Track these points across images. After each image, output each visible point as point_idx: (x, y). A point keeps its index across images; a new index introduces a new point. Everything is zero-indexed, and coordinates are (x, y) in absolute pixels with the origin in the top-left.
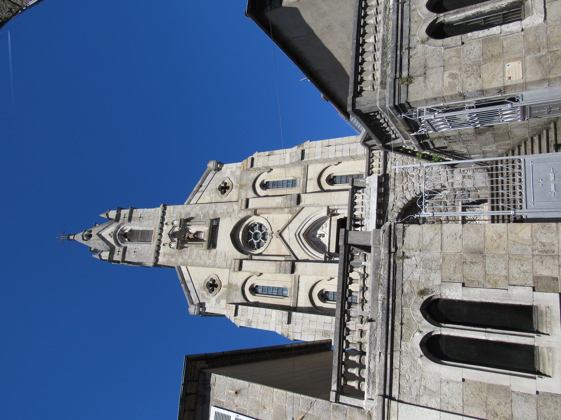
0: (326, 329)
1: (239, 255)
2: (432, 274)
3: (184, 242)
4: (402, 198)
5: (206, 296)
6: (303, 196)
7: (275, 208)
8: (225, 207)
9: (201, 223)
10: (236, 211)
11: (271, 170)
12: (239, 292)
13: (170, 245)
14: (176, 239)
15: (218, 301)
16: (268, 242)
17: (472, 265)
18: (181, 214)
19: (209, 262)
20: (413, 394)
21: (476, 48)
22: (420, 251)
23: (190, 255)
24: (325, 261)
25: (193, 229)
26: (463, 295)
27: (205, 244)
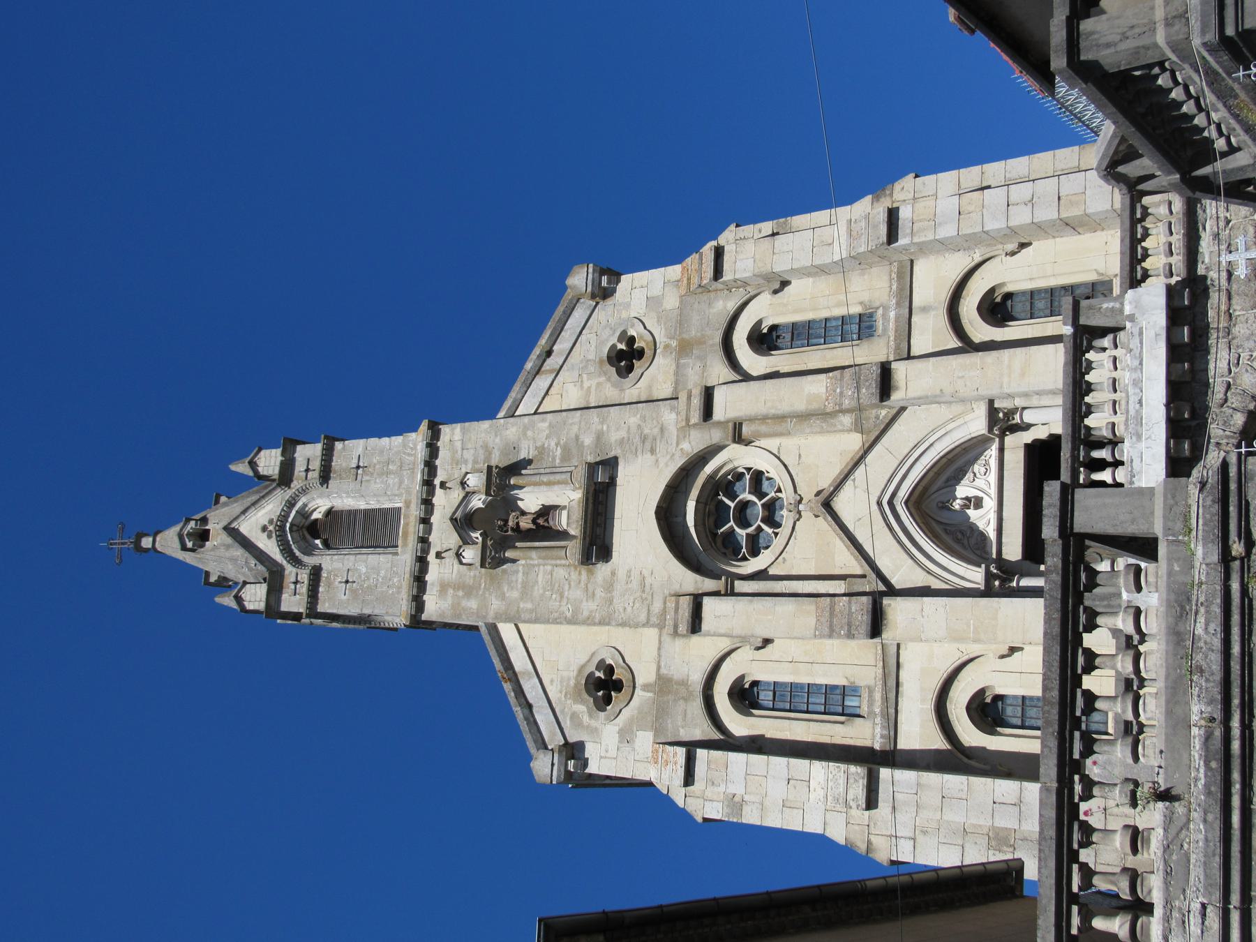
9: (558, 477)
13: (458, 555)
14: (476, 535)
25: (531, 500)
27: (574, 548)
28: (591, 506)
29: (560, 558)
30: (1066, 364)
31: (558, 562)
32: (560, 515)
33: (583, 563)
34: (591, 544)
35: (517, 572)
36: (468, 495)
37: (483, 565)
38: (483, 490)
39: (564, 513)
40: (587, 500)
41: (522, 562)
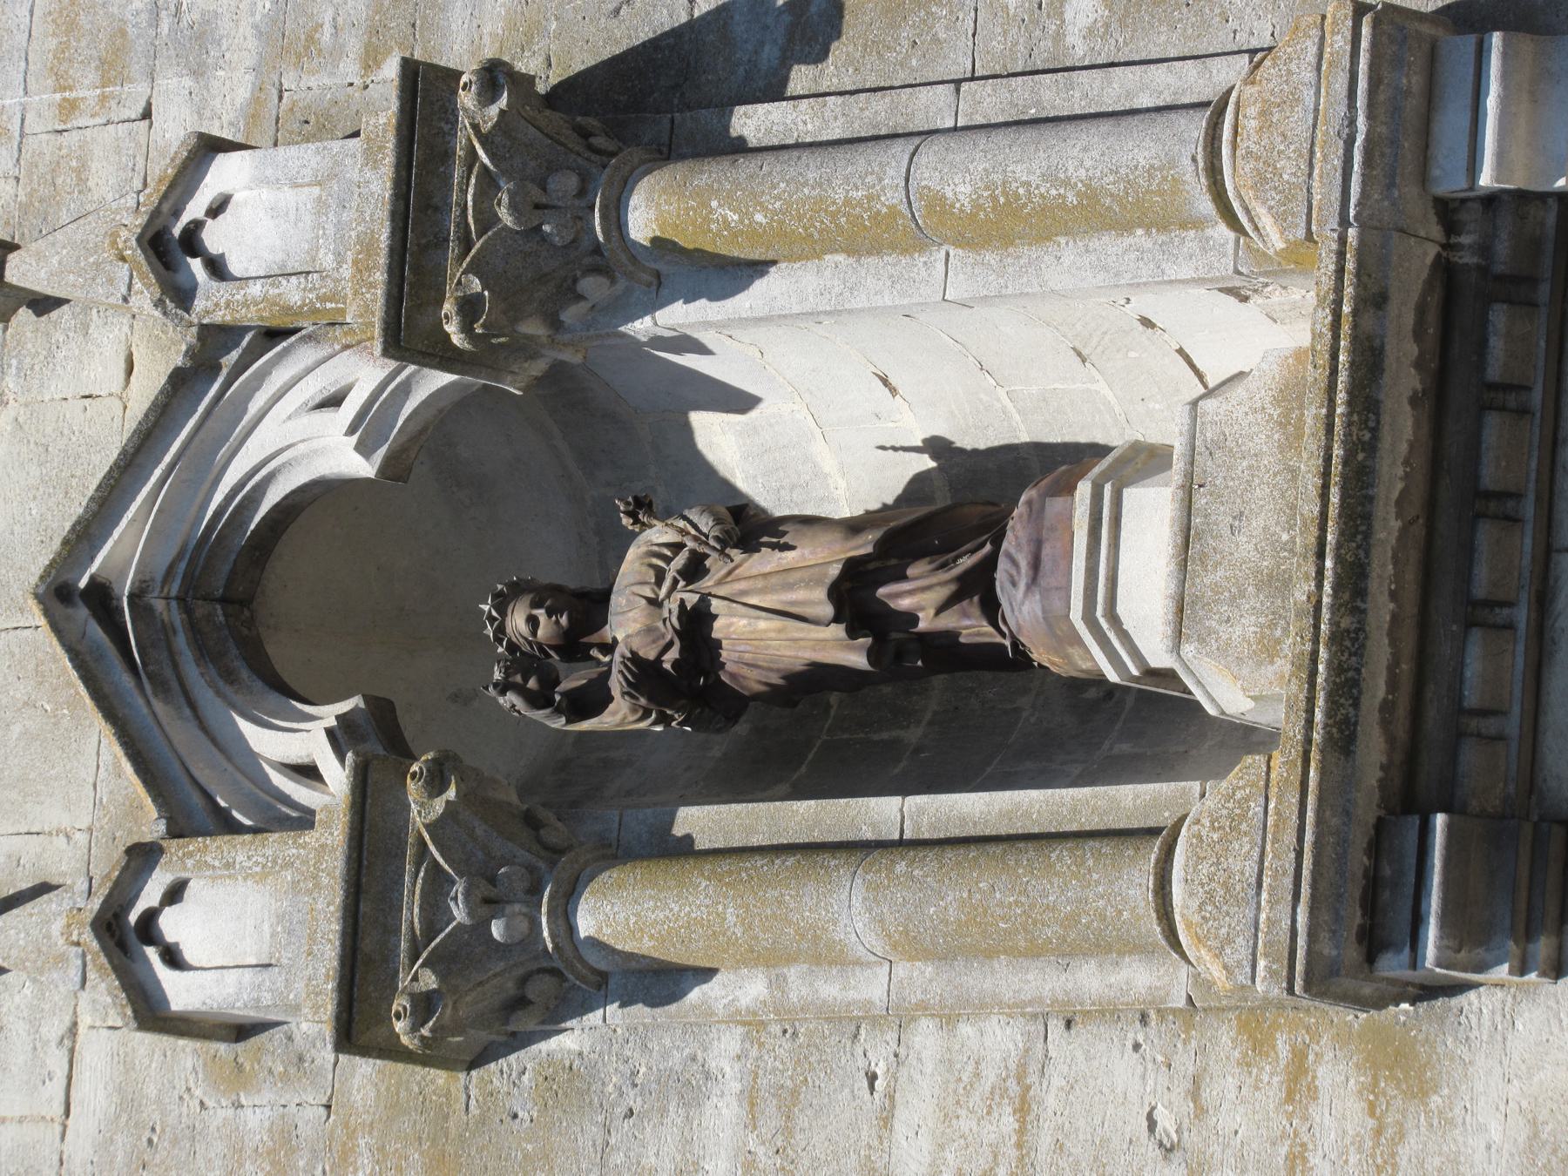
3: (571, 818)
9: (1083, 159)
13: (125, 938)
14: (296, 743)
25: (817, 395)
27: (1241, 839)
28: (1402, 427)
29: (1108, 945)
30: (307, 786)
31: (1091, 980)
32: (1107, 526)
33: (1322, 980)
34: (1408, 799)
35: (690, 1087)
36: (216, 363)
37: (356, 1029)
38: (367, 302)
39: (1149, 513)
40: (1370, 361)
41: (737, 990)
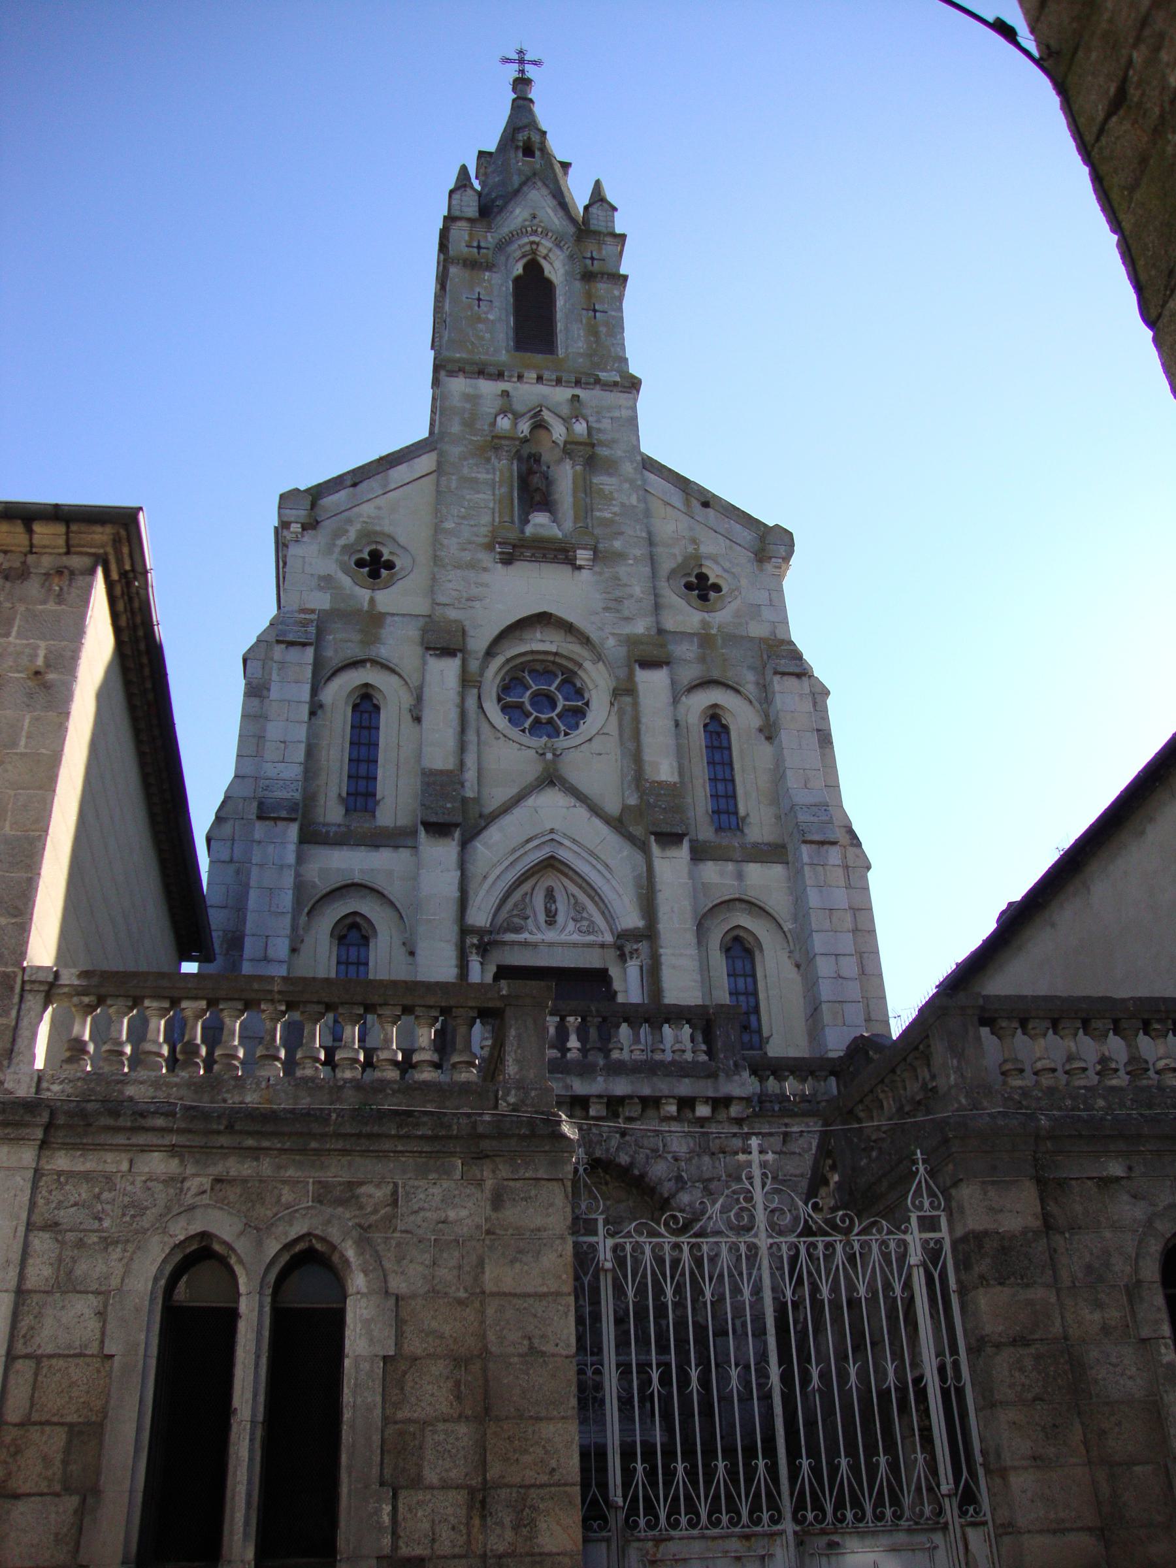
0: (248, 942)
1: (479, 642)
2: (420, 1268)
4: (679, 1178)
5: (342, 542)
6: (683, 852)
7: (637, 757)
8: (637, 590)
10: (627, 630)
11: (769, 738)
12: (353, 651)
15: (326, 582)
16: (526, 739)
17: (450, 1384)
18: (607, 444)
19: (452, 545)
20: (62, 1213)
21: (1130, 1383)
22: (488, 1232)
23: (475, 481)
24: (465, 931)
26: (357, 1358)
